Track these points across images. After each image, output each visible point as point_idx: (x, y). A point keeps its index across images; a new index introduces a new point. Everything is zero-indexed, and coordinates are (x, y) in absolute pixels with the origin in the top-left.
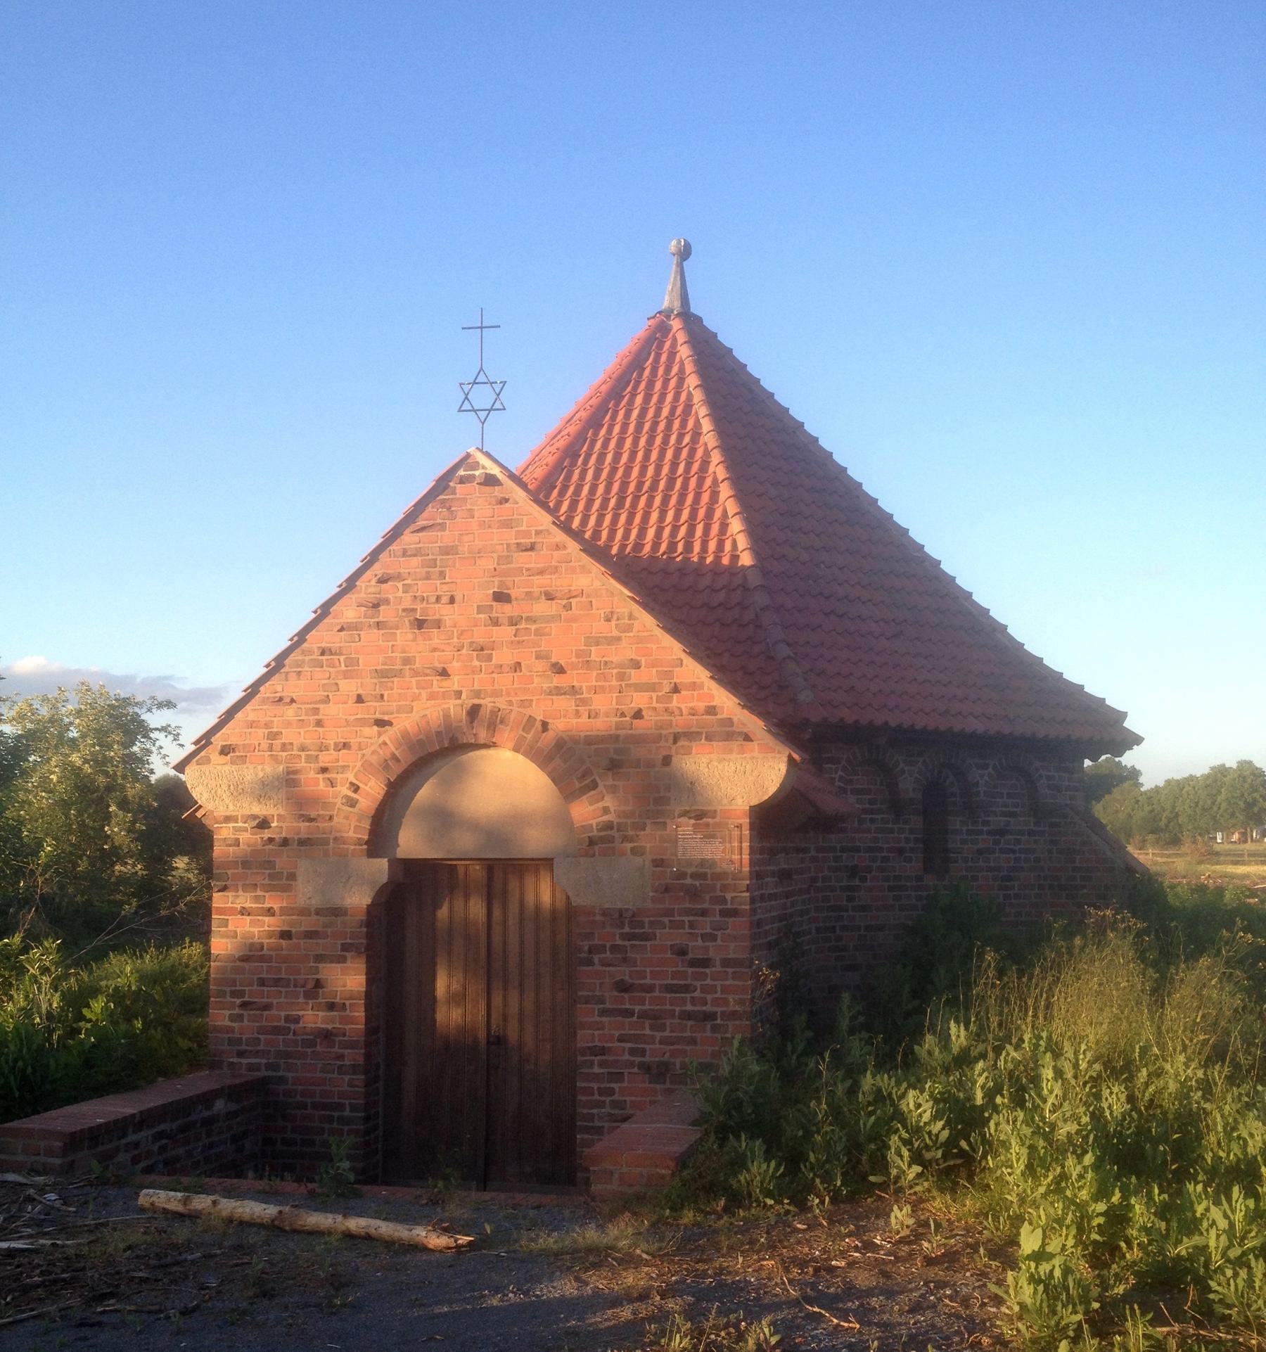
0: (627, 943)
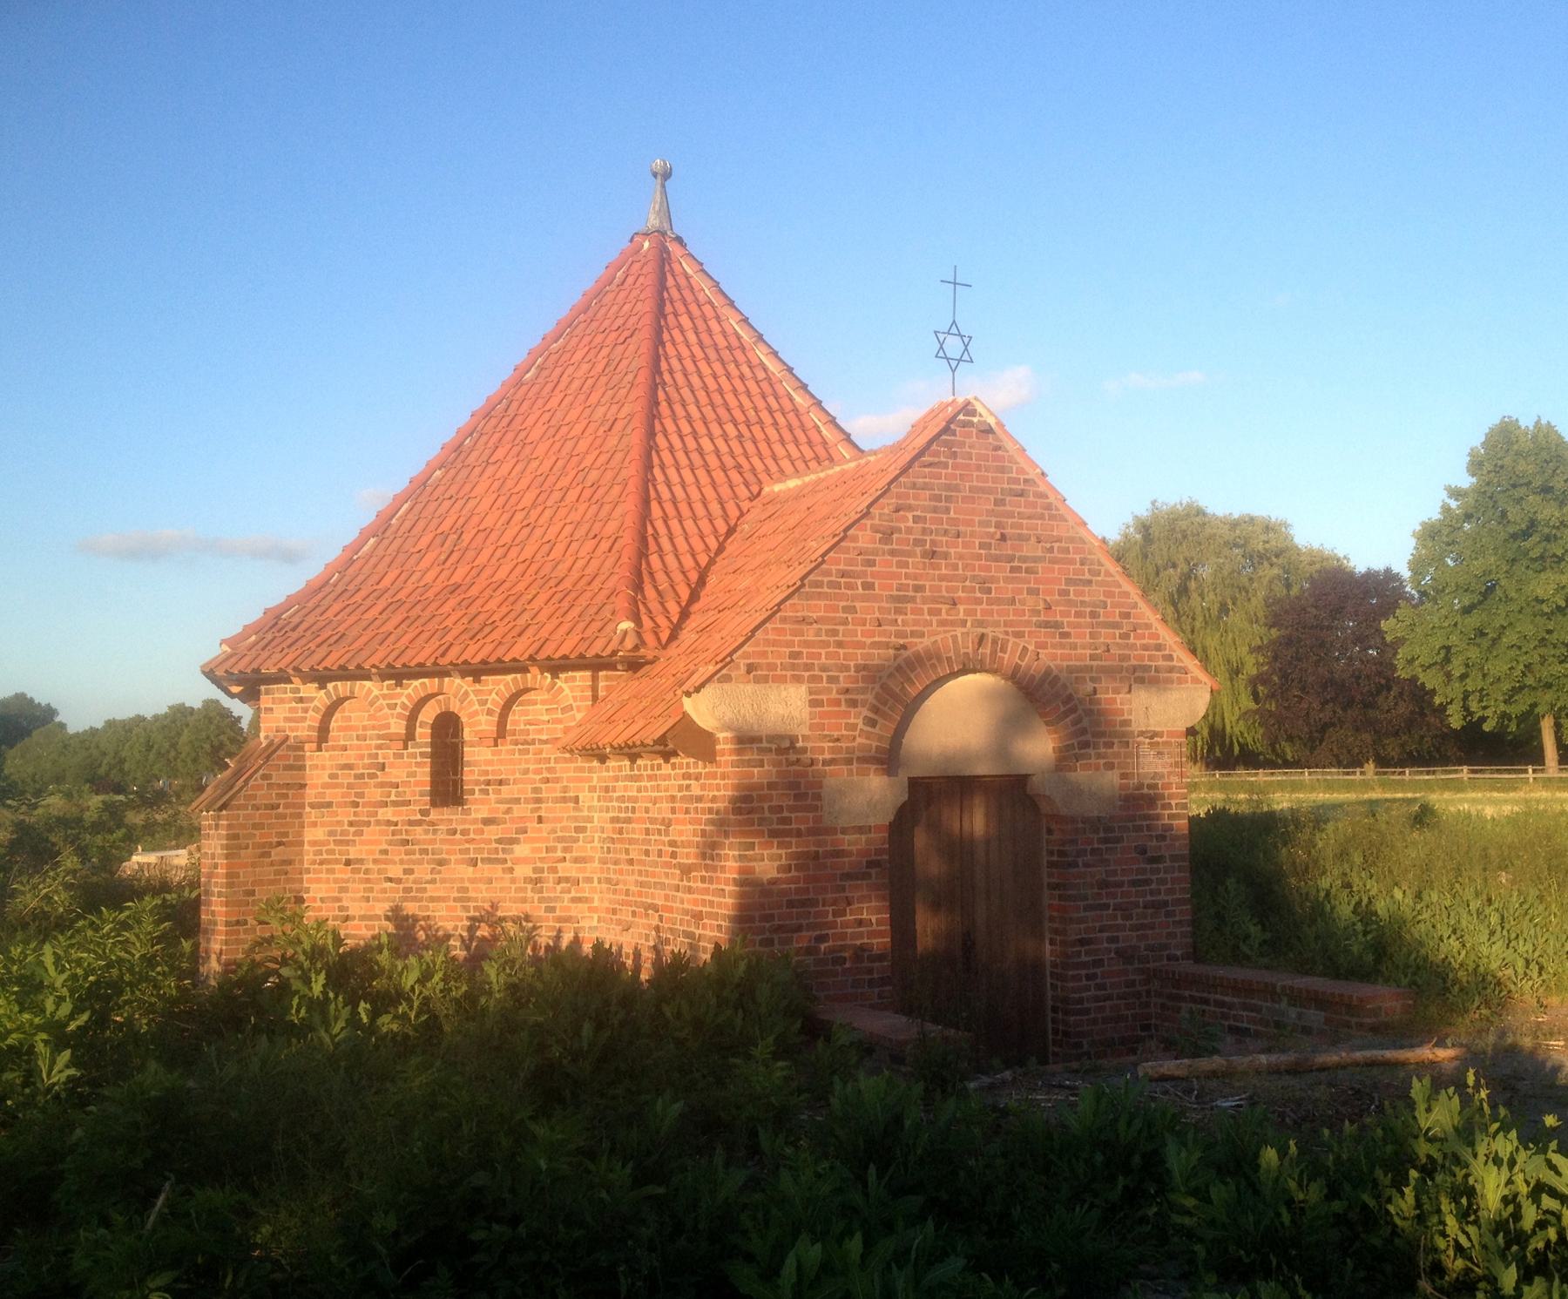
0: (1103, 847)
